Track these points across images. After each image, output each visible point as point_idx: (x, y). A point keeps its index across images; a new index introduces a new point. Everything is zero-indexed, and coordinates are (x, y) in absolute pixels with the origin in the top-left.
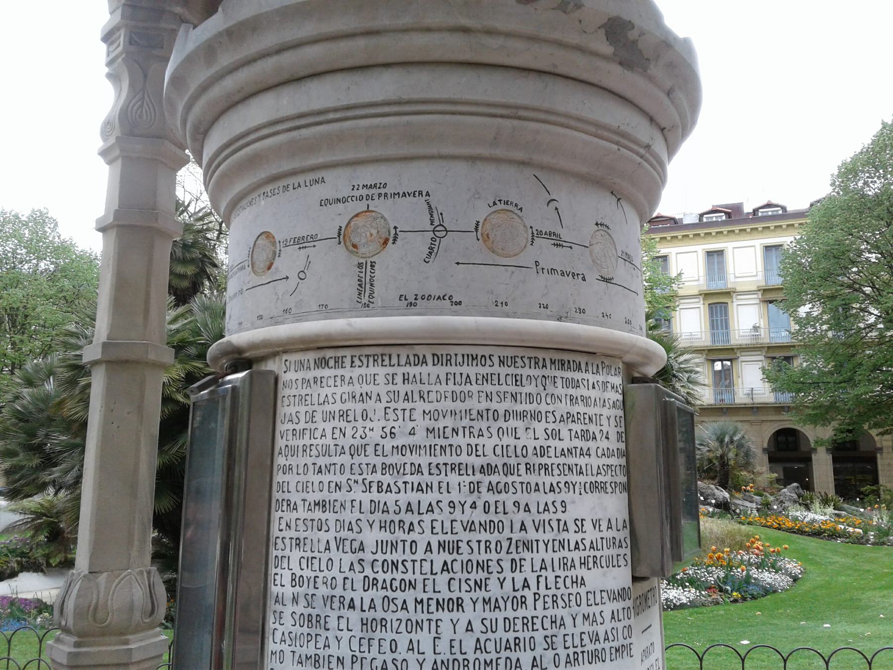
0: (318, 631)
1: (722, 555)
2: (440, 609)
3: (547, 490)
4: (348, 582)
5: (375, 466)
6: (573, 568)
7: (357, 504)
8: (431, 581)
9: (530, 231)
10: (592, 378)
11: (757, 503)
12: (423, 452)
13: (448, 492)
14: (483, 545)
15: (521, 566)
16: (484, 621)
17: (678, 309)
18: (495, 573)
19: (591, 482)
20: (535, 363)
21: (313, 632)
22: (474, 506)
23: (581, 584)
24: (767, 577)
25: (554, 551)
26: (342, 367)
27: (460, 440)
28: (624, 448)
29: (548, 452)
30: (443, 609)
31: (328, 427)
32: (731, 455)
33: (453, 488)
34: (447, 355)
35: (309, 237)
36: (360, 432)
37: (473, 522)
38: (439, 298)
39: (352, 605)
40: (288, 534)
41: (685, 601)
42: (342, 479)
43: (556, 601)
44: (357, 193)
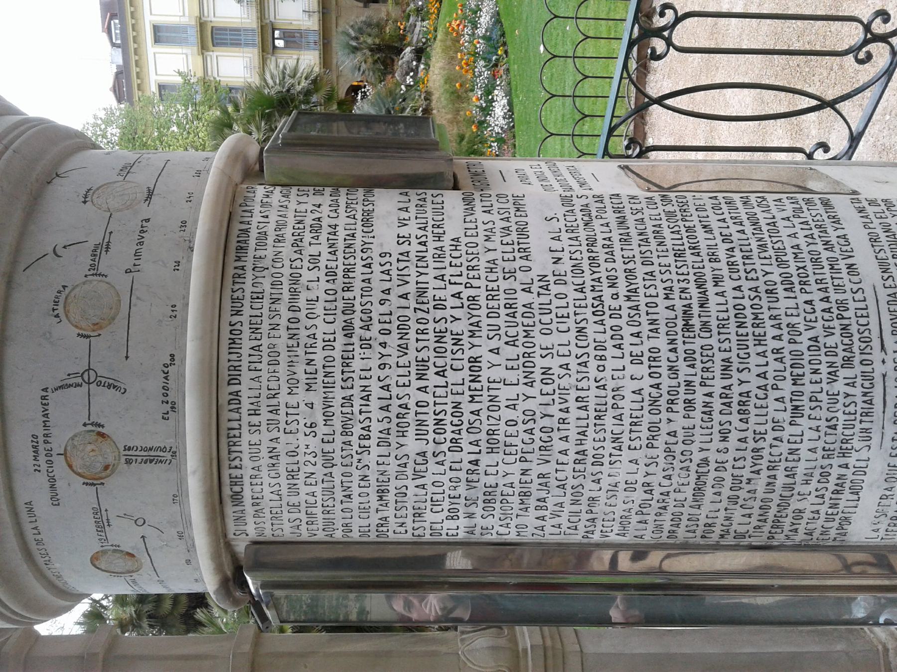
0: (498, 493)
1: (464, 61)
2: (479, 379)
3: (369, 270)
4: (454, 466)
6: (443, 249)
7: (381, 460)
8: (453, 387)
9: (90, 278)
10: (257, 218)
11: (416, 21)
12: (331, 395)
13: (370, 370)
14: (420, 337)
15: (440, 300)
16: (490, 337)
17: (218, 79)
19: (363, 225)
20: (239, 277)
22: (384, 345)
23: (458, 241)
24: (485, 20)
25: (427, 267)
26: (242, 478)
28: (330, 189)
29: (331, 268)
30: (479, 376)
31: (304, 490)
32: (370, 41)
33: (367, 365)
34: (229, 370)
35: (96, 516)
36: (310, 458)
37: (399, 346)
38: (166, 378)
39: (475, 463)
40: (409, 525)
41: (505, 101)
42: (356, 474)
43: (473, 267)
44: (44, 467)
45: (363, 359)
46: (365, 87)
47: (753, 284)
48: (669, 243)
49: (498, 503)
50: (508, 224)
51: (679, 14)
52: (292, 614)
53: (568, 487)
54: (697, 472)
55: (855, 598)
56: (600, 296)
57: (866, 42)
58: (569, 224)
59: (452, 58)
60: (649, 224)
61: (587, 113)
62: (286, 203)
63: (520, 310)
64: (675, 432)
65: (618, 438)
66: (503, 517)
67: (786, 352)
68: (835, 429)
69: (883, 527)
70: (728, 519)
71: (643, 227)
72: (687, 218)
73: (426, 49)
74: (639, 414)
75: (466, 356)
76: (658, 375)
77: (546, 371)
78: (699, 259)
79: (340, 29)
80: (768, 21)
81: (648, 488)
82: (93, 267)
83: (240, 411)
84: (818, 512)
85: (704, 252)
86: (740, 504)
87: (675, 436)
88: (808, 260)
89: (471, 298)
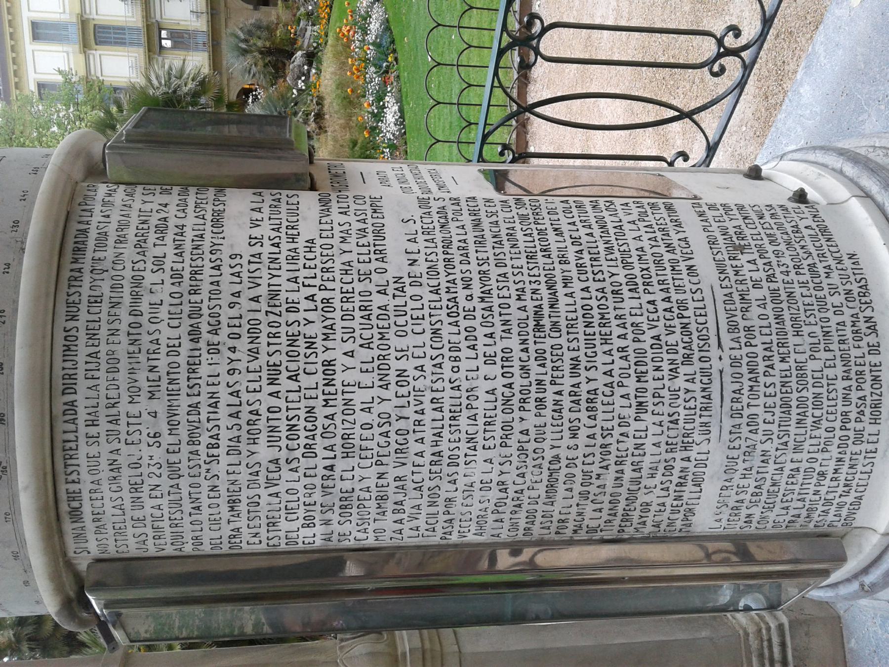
0: (355, 498)
3: (218, 273)
4: (309, 472)
5: (191, 453)
10: (97, 217)
12: (175, 403)
13: (218, 375)
14: (272, 341)
15: (293, 303)
17: (101, 78)
18: (299, 329)
19: (212, 226)
20: (75, 280)
22: (233, 349)
24: (374, 26)
27: (162, 364)
30: (333, 379)
31: (149, 503)
32: (260, 43)
33: (215, 370)
34: (64, 379)
36: (153, 469)
37: (249, 350)
40: (264, 535)
41: (396, 108)
42: (205, 485)
45: (210, 364)
46: (256, 90)
47: (600, 285)
48: (521, 245)
49: (355, 508)
50: (364, 226)
51: (545, 25)
52: (184, 630)
53: (425, 489)
54: (549, 469)
55: (722, 586)
56: (455, 298)
57: (719, 56)
58: (425, 226)
59: (344, 64)
60: (503, 227)
61: (472, 121)
62: (130, 202)
64: (528, 430)
65: (473, 439)
66: (360, 522)
67: (630, 350)
68: (677, 424)
69: (725, 517)
70: (580, 514)
71: (497, 229)
72: (539, 221)
73: (317, 53)
74: (492, 413)
75: (320, 360)
76: (510, 375)
77: (401, 373)
78: (550, 261)
79: (229, 31)
80: (637, 34)
83: (76, 421)
84: (664, 504)
85: (554, 254)
86: (590, 499)
87: (527, 434)
88: (651, 261)
89: (325, 301)
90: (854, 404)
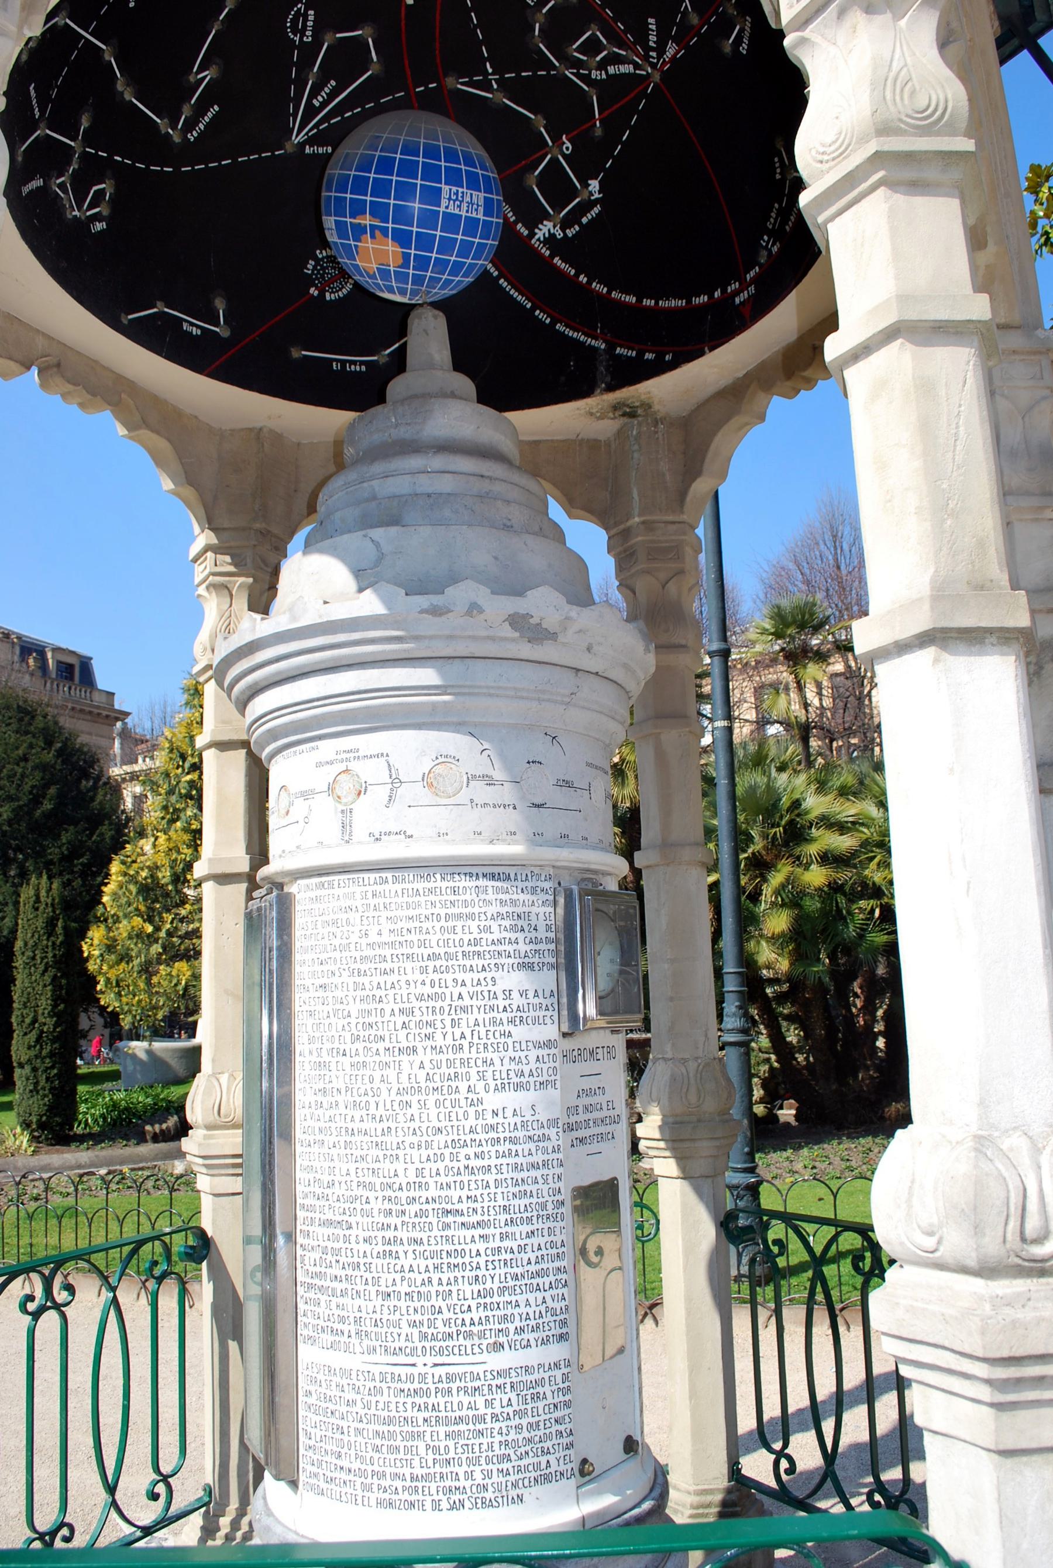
7: (345, 985)
14: (430, 1010)
21: (322, 1073)
22: (423, 983)
31: (326, 931)
40: (305, 1008)
42: (333, 968)
44: (339, 757)
47: (483, 1266)
48: (516, 1202)
58: (529, 1124)
60: (534, 1188)
63: (454, 1084)
67: (430, 1288)
75: (417, 1044)
77: (408, 1104)
78: (502, 1224)
81: (331, 1185)
82: (474, 777)
90: (392, 1483)
